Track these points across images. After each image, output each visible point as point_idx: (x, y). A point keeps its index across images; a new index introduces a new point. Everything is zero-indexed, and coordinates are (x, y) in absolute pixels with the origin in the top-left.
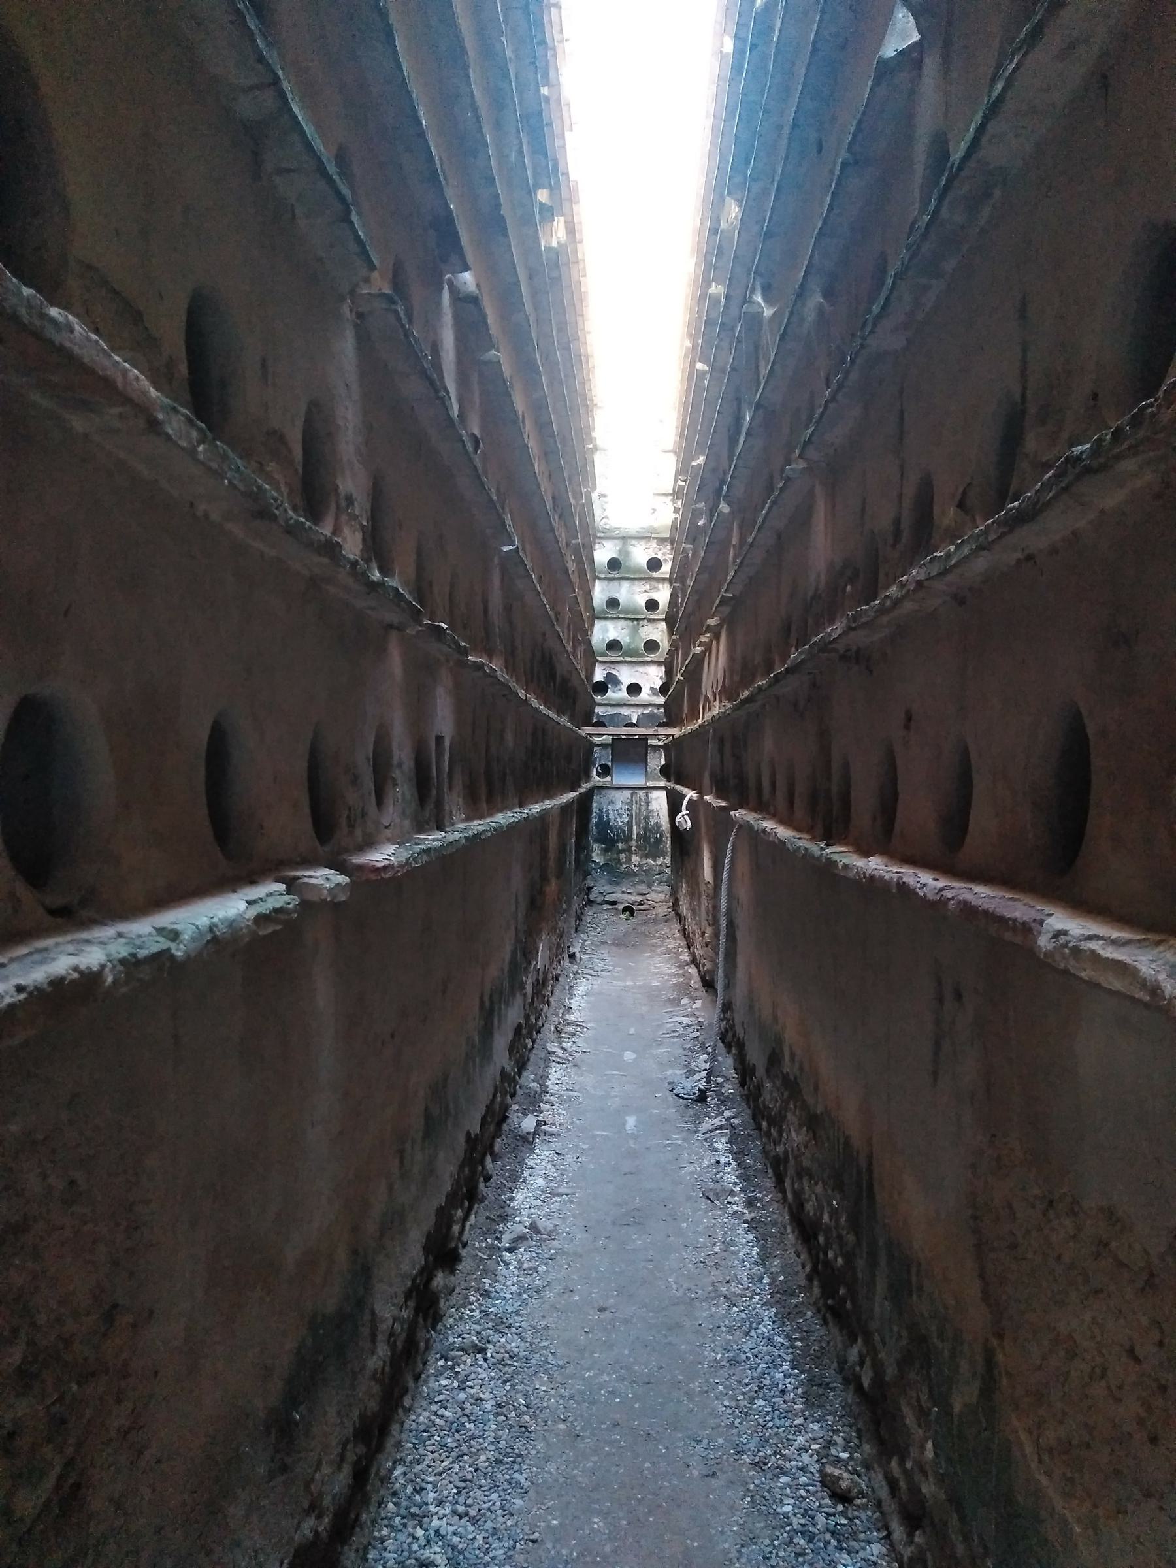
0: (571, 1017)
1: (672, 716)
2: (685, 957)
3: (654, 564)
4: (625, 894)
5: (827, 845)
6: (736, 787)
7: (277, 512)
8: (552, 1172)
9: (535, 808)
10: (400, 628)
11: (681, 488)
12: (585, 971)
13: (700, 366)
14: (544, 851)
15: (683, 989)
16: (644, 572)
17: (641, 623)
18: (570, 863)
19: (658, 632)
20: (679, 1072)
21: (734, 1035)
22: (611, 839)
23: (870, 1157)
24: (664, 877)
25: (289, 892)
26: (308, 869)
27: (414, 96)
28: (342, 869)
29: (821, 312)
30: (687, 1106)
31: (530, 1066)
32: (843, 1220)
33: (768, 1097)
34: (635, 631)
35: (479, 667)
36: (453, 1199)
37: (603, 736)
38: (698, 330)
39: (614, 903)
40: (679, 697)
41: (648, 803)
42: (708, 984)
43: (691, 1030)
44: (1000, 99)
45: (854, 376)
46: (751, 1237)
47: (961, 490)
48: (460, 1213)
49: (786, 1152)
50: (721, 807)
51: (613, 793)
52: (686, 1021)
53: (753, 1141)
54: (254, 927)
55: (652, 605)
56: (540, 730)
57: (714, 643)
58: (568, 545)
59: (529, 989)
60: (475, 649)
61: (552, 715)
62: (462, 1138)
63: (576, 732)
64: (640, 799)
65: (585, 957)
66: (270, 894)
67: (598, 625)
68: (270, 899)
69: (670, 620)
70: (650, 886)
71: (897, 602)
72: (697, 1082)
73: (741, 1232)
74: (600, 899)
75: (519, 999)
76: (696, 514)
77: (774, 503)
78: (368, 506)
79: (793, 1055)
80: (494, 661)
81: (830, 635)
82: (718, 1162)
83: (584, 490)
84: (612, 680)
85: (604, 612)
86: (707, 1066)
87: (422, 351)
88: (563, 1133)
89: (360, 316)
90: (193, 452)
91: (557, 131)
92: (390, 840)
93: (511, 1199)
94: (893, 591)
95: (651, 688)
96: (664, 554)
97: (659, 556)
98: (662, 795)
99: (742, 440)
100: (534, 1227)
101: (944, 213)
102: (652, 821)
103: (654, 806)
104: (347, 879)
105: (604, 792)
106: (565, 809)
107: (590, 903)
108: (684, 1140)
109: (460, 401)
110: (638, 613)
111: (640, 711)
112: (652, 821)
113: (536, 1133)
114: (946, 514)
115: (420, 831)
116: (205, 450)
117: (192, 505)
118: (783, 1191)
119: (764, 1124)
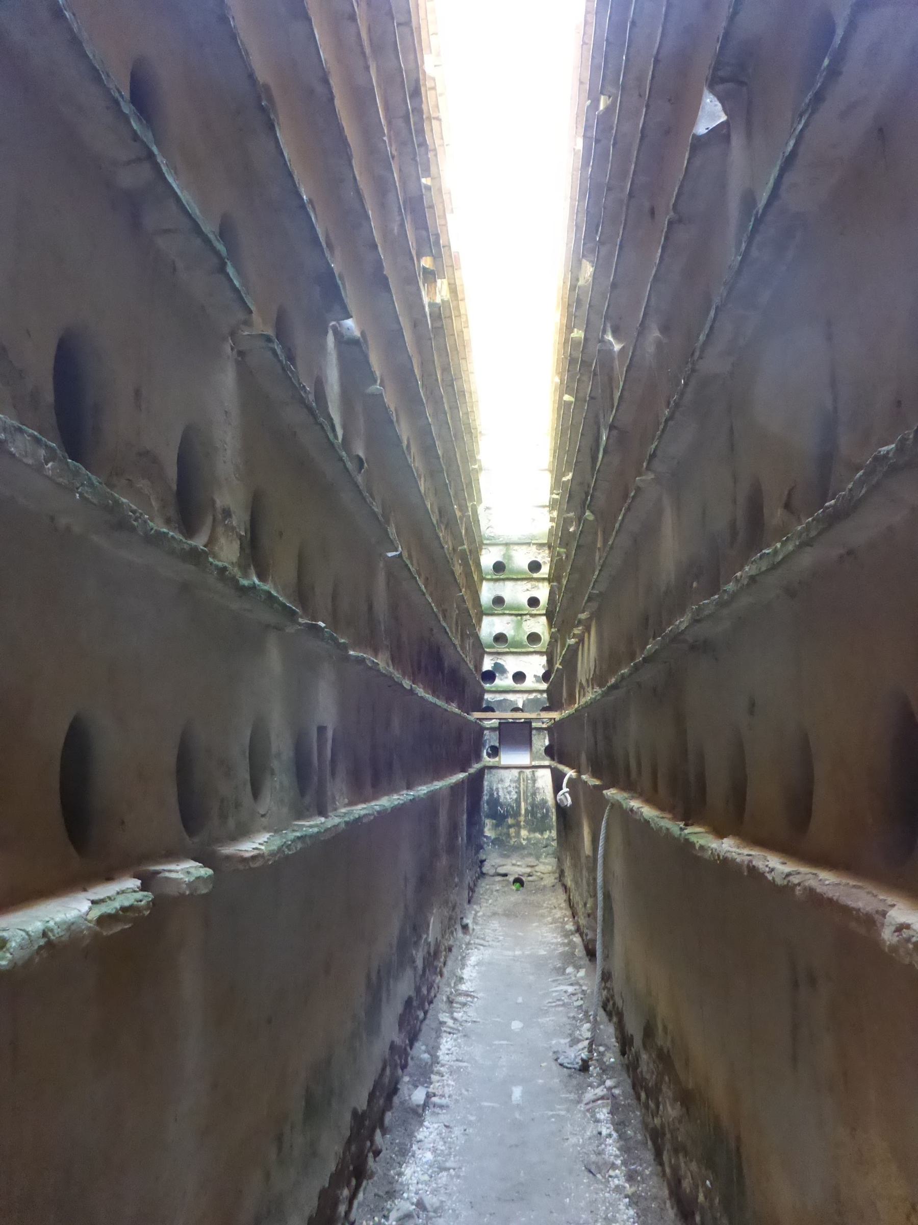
0: (463, 987)
1: (553, 704)
2: (570, 927)
3: (535, 566)
4: (515, 867)
5: (686, 825)
6: (609, 768)
7: (135, 523)
8: (441, 1146)
9: (423, 790)
10: (278, 628)
11: (554, 501)
12: (477, 941)
13: (567, 398)
14: (433, 830)
15: (569, 958)
16: (526, 573)
17: (524, 617)
18: (462, 840)
19: (539, 625)
20: (563, 1041)
21: (614, 1004)
22: (501, 813)
23: (738, 1139)
24: (550, 850)
25: (144, 888)
26: (170, 862)
27: (295, 177)
28: (205, 859)
29: (659, 345)
30: (570, 1076)
31: (422, 1037)
32: (717, 1201)
33: (645, 1069)
34: (519, 625)
35: (362, 661)
36: (338, 1179)
37: (491, 721)
38: (563, 368)
39: (505, 875)
40: (559, 682)
41: (534, 781)
42: (591, 953)
43: (575, 998)
44: (794, 153)
45: (689, 396)
46: (631, 1212)
47: (786, 493)
48: (346, 1192)
49: (662, 1126)
50: (595, 786)
51: (502, 772)
52: (571, 989)
53: (634, 1112)
54: (98, 929)
55: (533, 602)
56: (428, 714)
57: (586, 635)
58: (454, 550)
59: (419, 963)
60: (358, 643)
61: (439, 703)
62: (348, 1117)
63: (464, 718)
64: (523, 776)
65: (477, 928)
66: (124, 891)
67: (486, 620)
68: (121, 897)
69: (549, 615)
70: (538, 858)
71: (734, 596)
72: (579, 1053)
73: (622, 1207)
74: (492, 871)
75: (409, 972)
76: (567, 522)
77: (628, 509)
78: (247, 518)
79: (665, 1028)
80: (380, 656)
81: (678, 627)
82: (600, 1133)
83: (469, 504)
84: (499, 669)
85: (492, 609)
86: (589, 1035)
87: (300, 384)
88: (452, 1105)
89: (241, 353)
90: (39, 468)
91: (438, 212)
92: (266, 829)
93: (400, 1174)
94: (731, 587)
95: (535, 676)
96: (543, 557)
97: (540, 560)
98: (548, 772)
99: (600, 456)
100: (420, 1205)
101: (754, 253)
102: (539, 798)
103: (539, 784)
104: (210, 872)
105: (494, 771)
106: (454, 788)
107: (483, 875)
108: (568, 1110)
109: (344, 427)
110: (522, 610)
111: (525, 696)
112: (539, 798)
113: (425, 1105)
114: (775, 515)
115: (299, 819)
116: (53, 469)
117: (52, 519)
118: (661, 1164)
119: (643, 1095)
